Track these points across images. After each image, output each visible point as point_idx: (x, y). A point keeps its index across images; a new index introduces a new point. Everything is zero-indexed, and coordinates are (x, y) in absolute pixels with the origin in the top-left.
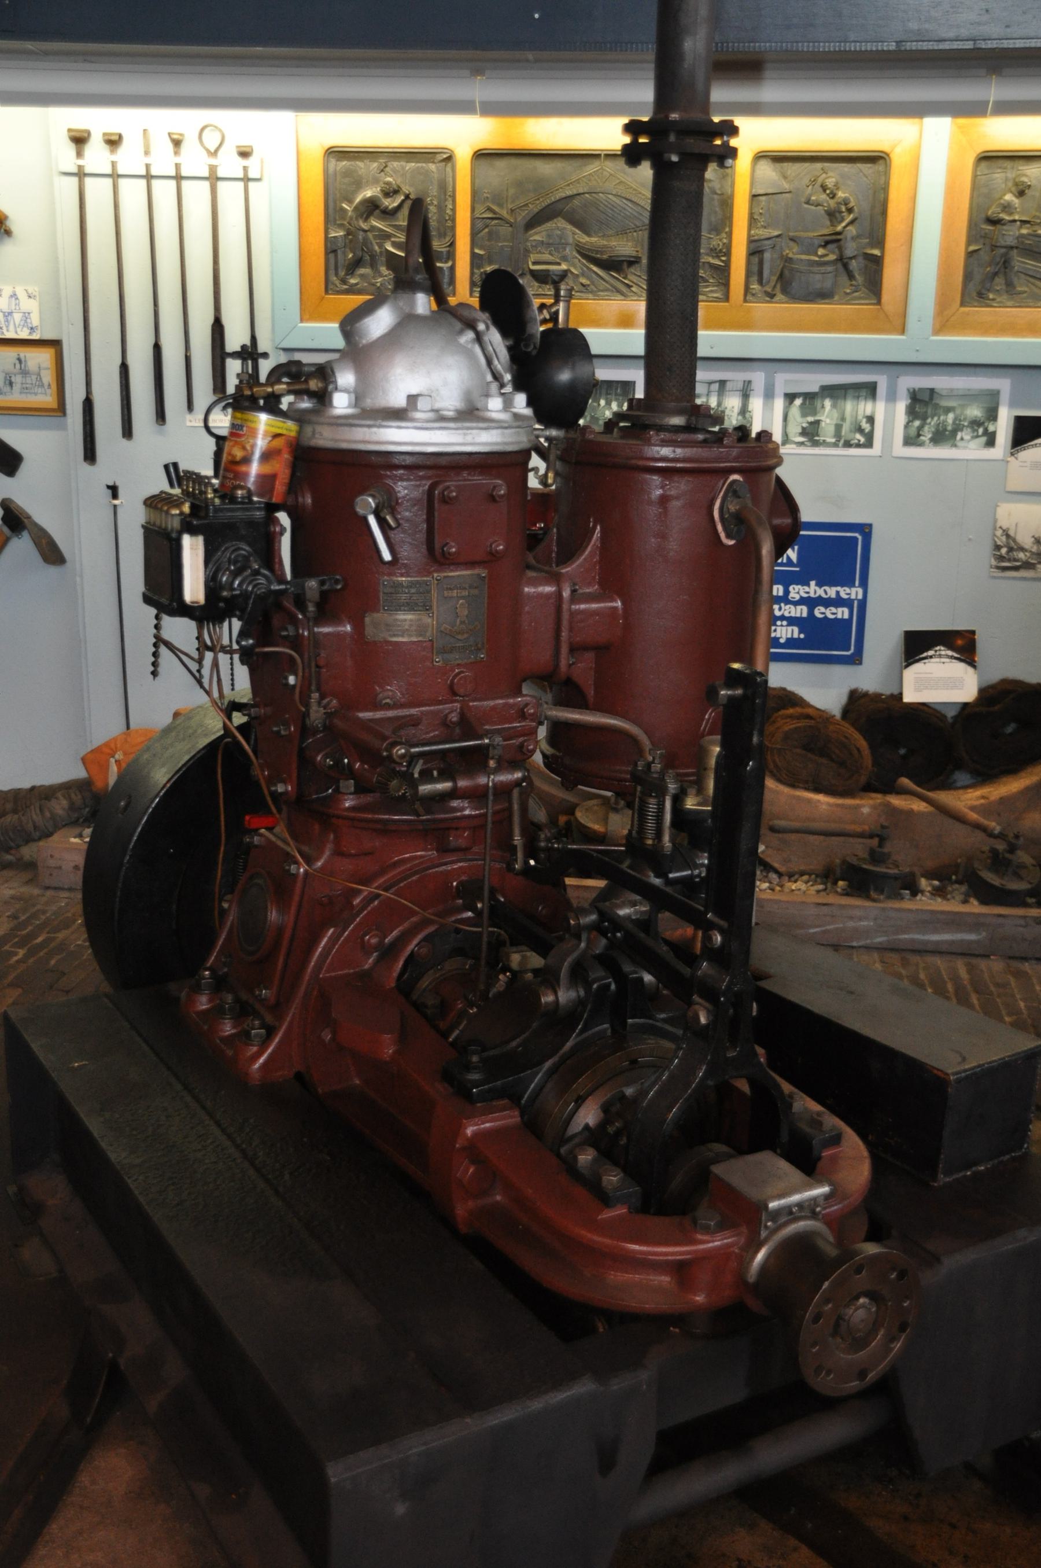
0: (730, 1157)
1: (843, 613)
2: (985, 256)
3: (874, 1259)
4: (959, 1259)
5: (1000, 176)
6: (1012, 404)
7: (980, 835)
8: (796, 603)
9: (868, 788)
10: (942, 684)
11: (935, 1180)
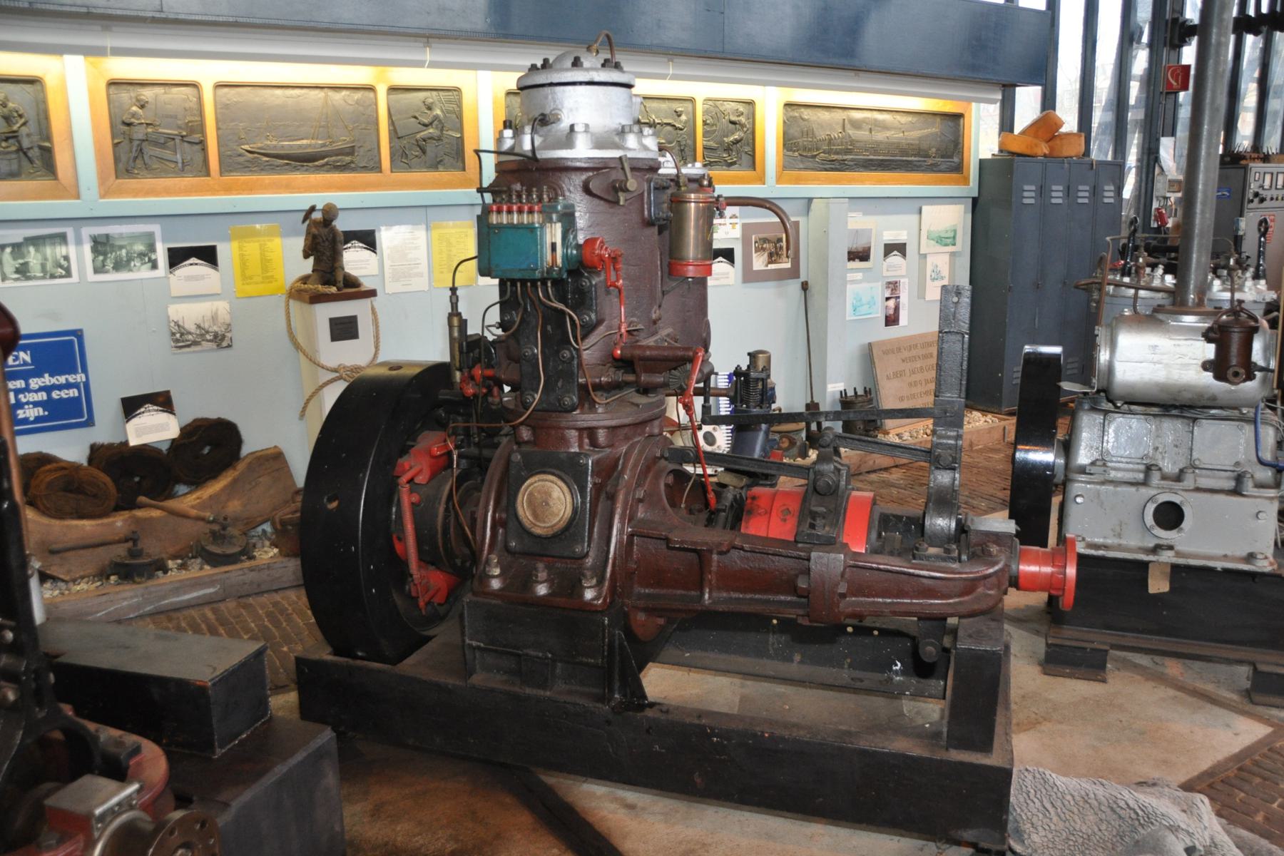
0: (58, 789)
1: (73, 393)
2: (125, 145)
3: (181, 821)
4: (245, 797)
5: (125, 96)
6: (164, 241)
7: (201, 523)
8: (36, 391)
9: (118, 508)
10: (154, 429)
11: (214, 753)
